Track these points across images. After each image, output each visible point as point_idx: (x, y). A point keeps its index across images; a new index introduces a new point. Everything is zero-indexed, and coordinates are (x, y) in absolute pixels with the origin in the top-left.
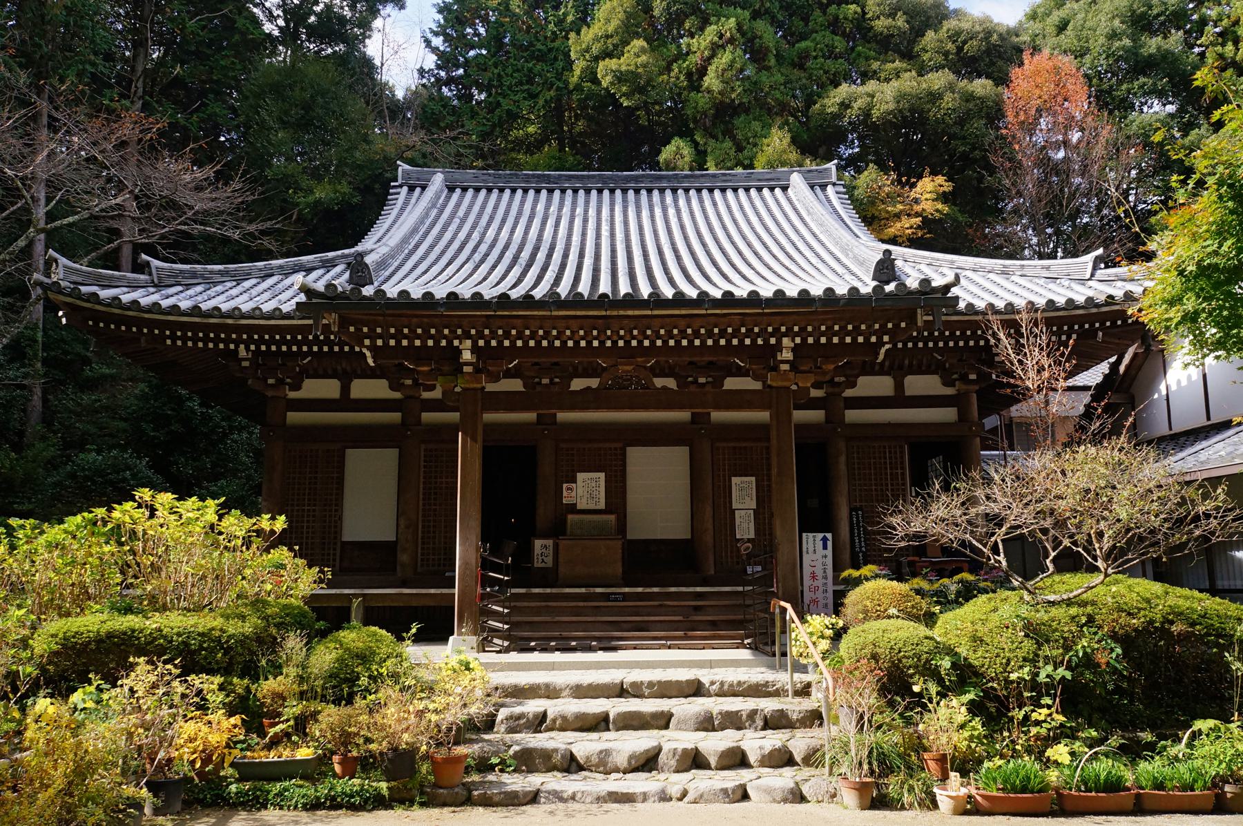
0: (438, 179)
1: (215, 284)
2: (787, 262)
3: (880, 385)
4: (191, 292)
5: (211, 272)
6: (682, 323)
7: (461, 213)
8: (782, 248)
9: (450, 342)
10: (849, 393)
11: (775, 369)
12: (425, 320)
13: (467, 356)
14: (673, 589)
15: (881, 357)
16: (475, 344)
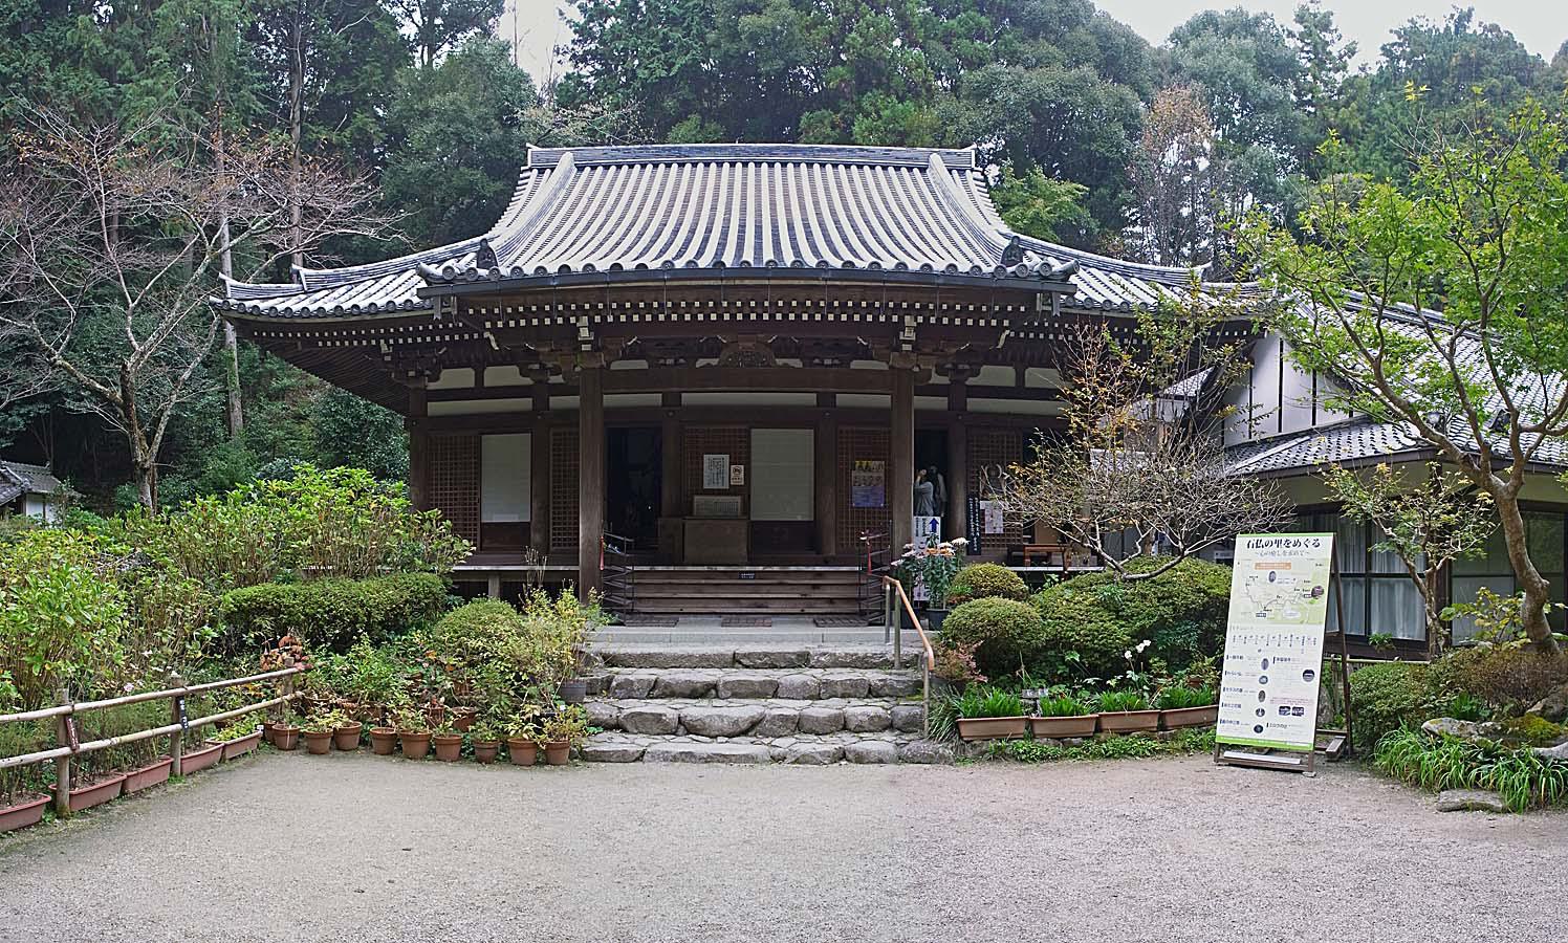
0: (567, 159)
1: (357, 284)
2: (919, 242)
3: (1005, 375)
4: (336, 294)
5: (352, 274)
6: (802, 294)
7: (589, 193)
8: (916, 229)
9: (567, 320)
10: (971, 381)
11: (898, 349)
12: (540, 297)
13: (584, 333)
14: (793, 568)
15: (1001, 343)
16: (591, 320)
